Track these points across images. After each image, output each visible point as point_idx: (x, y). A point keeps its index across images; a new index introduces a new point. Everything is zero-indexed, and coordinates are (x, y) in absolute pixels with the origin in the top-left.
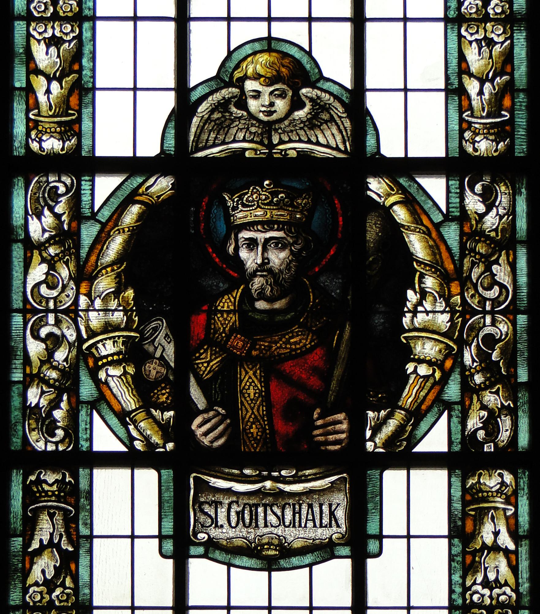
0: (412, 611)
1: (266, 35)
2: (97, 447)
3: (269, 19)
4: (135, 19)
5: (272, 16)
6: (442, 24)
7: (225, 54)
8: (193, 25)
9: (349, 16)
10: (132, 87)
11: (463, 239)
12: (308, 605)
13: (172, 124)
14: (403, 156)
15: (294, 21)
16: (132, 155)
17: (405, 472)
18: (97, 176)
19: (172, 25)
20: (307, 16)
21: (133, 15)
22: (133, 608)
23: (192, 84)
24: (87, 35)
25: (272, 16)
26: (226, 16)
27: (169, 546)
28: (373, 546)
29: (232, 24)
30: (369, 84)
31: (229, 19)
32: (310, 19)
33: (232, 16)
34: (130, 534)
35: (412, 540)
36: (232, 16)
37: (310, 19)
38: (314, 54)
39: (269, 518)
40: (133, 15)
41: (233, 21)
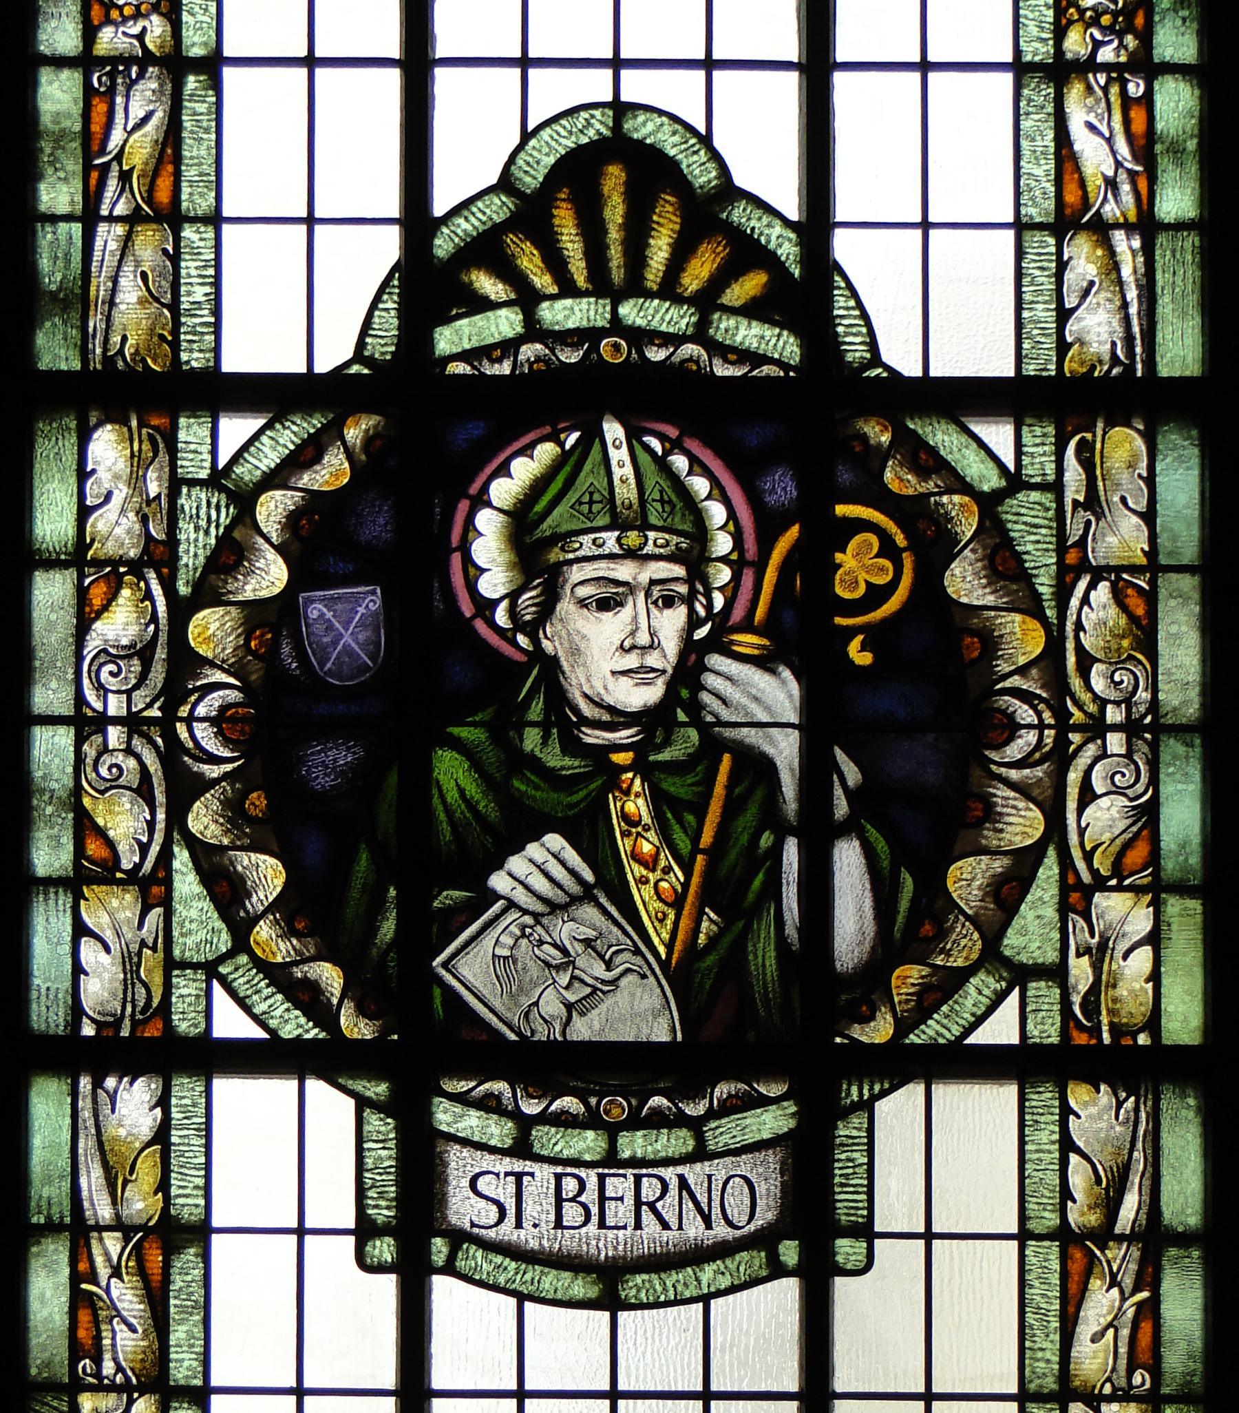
0: (622, 1403)
3: (617, 63)
4: (311, 62)
5: (715, 57)
6: (1008, 78)
7: (516, 140)
8: (441, 75)
10: (918, 219)
12: (607, 1388)
13: (390, 303)
14: (304, 370)
16: (304, 371)
19: (791, 81)
20: (702, 57)
21: (519, 55)
22: (928, 1397)
23: (439, 209)
26: (702, 57)
27: (384, 1249)
28: (847, 1250)
29: (320, 72)
32: (709, 64)
33: (624, 55)
35: (308, 1239)
36: (532, 54)
37: (709, 64)
38: (717, 143)
40: (519, 55)
41: (933, 70)
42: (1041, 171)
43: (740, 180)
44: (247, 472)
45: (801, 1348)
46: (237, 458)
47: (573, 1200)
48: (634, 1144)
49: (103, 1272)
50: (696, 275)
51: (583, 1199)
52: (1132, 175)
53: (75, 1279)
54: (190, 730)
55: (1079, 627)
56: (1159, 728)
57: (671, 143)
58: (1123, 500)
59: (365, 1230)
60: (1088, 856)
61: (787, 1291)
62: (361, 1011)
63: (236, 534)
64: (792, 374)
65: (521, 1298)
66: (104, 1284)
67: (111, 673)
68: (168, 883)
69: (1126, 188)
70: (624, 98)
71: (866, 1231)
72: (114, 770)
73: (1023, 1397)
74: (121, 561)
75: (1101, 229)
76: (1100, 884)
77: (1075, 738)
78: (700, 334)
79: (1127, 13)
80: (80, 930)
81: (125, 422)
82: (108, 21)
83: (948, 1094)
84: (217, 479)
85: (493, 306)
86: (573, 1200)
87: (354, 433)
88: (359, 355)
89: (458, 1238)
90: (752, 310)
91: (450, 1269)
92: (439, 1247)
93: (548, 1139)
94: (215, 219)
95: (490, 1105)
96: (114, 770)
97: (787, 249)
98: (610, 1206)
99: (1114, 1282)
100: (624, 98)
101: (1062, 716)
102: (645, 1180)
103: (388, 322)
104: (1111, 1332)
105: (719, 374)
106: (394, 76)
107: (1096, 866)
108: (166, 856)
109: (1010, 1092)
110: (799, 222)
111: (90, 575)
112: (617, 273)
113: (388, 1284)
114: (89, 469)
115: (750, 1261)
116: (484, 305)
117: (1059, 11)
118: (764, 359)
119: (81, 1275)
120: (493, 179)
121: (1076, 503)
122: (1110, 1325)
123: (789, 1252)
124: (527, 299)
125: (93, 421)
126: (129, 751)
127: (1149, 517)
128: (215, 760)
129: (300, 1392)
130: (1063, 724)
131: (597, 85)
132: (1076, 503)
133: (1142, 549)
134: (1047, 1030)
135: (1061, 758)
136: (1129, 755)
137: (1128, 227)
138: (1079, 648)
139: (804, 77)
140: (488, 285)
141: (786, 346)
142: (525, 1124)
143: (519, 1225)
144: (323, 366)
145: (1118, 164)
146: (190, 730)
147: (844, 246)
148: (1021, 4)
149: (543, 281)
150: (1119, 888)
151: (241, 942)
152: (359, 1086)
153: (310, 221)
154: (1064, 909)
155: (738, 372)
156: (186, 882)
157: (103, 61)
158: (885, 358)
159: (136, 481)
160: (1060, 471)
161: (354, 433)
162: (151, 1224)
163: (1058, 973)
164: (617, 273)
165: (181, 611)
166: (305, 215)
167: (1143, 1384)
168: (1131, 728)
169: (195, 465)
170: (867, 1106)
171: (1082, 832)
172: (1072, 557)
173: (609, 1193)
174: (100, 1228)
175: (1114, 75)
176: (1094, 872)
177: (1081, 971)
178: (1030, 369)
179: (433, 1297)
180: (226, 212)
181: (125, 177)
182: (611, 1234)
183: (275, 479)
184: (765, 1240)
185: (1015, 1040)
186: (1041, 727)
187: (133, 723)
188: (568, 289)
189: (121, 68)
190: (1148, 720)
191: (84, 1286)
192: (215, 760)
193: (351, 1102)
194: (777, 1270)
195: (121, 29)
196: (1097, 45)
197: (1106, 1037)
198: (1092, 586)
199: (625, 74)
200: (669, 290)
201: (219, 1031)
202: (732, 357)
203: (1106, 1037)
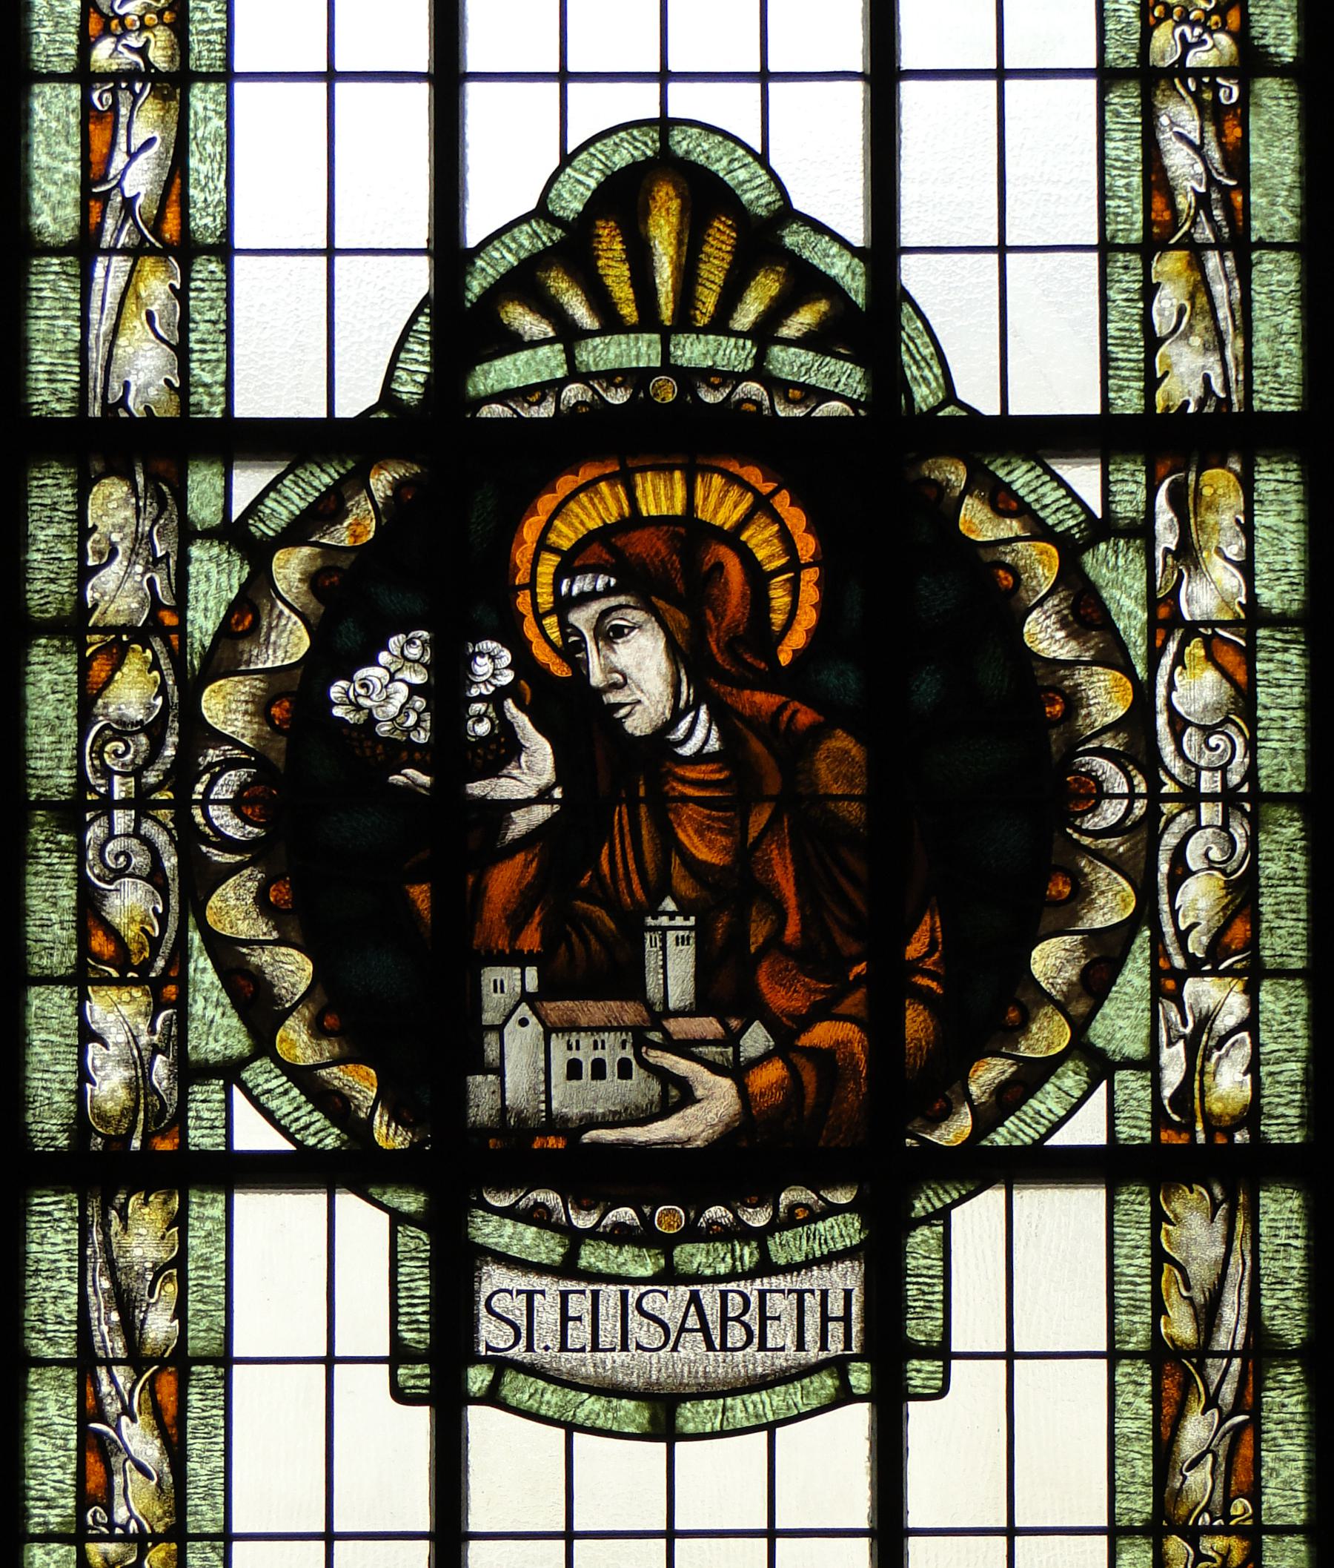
1: (656, 114)
3: (664, 76)
7: (555, 162)
9: (426, 70)
11: (1206, 629)
14: (323, 414)
17: (321, 1198)
21: (325, 69)
23: (472, 240)
24: (206, 125)
26: (757, 69)
28: (920, 1372)
30: (908, 236)
31: (564, 77)
33: (1008, 65)
34: (324, 1354)
38: (774, 162)
39: (632, 1325)
40: (325, 69)
42: (1129, 182)
43: (797, 205)
47: (737, 1319)
48: (694, 1256)
49: (113, 1408)
50: (748, 313)
51: (746, 1318)
53: (83, 1418)
54: (206, 814)
56: (1258, 797)
57: (719, 161)
59: (399, 1354)
60: (1182, 937)
61: (858, 1418)
62: (396, 1117)
64: (862, 412)
65: (571, 1428)
67: (115, 752)
68: (183, 982)
70: (662, 1446)
71: (942, 1352)
72: (122, 859)
76: (1194, 968)
77: (1167, 808)
78: (759, 372)
79: (1221, 10)
80: (87, 1035)
81: (128, 476)
82: (106, 31)
83: (1030, 1200)
85: (534, 344)
86: (737, 1319)
87: (381, 483)
89: (501, 1365)
90: (811, 341)
91: (493, 1397)
92: (478, 1378)
95: (537, 1217)
96: (122, 859)
98: (772, 1328)
99: (128, 204)
102: (730, 1295)
103: (420, 355)
104: (1210, 1457)
105: (782, 414)
107: (1191, 951)
108: (181, 953)
109: (1096, 1197)
111: (92, 644)
113: (421, 1416)
114: (90, 525)
115: (826, 1384)
117: (1144, 11)
119: (89, 1411)
120: (531, 204)
121: (1167, 551)
122: (1208, 1451)
123: (860, 1378)
124: (569, 334)
125: (97, 466)
126: (136, 834)
127: (1246, 568)
129: (771, 1534)
130: (1155, 797)
131: (643, 102)
132: (1167, 551)
133: (1240, 603)
134: (1136, 1130)
135: (1150, 827)
136: (1225, 827)
137: (1220, 246)
138: (1174, 716)
142: (575, 1238)
143: (530, 1348)
144: (348, 408)
145: (1211, 181)
146: (206, 814)
147: (913, 273)
148: (1107, 6)
150: (1215, 973)
151: (263, 1045)
152: (391, 1198)
153: (330, 252)
154: (1157, 993)
157: (105, 77)
158: (961, 395)
161: (381, 483)
162: (167, 1355)
163: (1150, 1065)
165: (191, 688)
166: (324, 246)
167: (100, 99)
168: (1228, 798)
170: (943, 1215)
171: (1174, 914)
172: (1163, 612)
173: (571, 1313)
174: (110, 1363)
175: (1206, 80)
176: (1189, 958)
179: (868, 1479)
182: (601, 1355)
183: (295, 533)
184: (838, 1366)
185: (1095, 409)
187: (141, 804)
188: (612, 323)
189: (124, 85)
190: (1245, 789)
191: (93, 1425)
193: (384, 1218)
194: (844, 1396)
196: (1187, 46)
197: (1201, 1138)
198: (1183, 644)
200: (720, 325)
201: (239, 1145)
203: (1201, 1138)
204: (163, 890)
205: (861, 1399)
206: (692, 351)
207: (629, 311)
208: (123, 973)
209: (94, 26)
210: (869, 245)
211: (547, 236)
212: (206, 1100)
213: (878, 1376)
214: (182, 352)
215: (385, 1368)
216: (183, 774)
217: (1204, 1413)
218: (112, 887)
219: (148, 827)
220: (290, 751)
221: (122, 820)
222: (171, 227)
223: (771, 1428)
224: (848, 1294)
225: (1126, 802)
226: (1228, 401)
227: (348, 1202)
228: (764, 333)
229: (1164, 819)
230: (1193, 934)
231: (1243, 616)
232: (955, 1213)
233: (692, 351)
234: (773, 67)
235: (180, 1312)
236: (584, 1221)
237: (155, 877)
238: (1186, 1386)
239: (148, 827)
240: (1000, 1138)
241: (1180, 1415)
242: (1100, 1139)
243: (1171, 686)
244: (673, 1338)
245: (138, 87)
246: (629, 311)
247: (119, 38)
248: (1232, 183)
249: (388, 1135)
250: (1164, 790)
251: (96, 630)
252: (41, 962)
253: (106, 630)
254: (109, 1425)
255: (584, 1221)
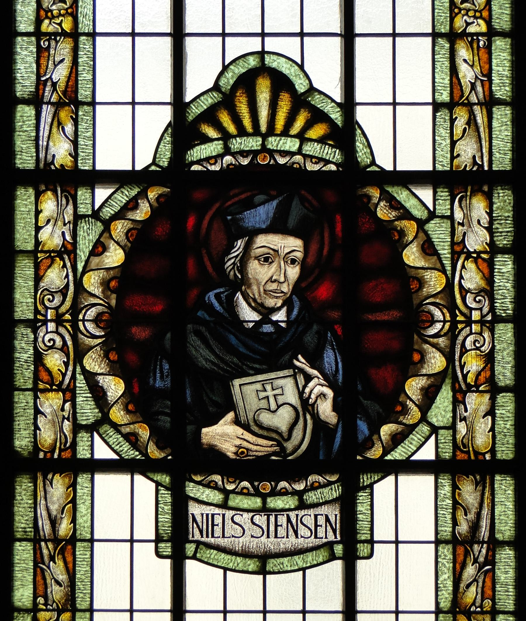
2: (97, 456)
3: (263, 35)
7: (220, 68)
12: (391, 32)
13: (168, 138)
15: (273, 36)
16: (131, 169)
18: (98, 188)
19: (168, 40)
23: (188, 99)
25: (266, 32)
27: (166, 548)
28: (363, 549)
29: (137, 39)
31: (224, 35)
35: (391, 101)
36: (226, 32)
38: (306, 68)
41: (99, 36)
44: (108, 212)
45: (343, 592)
46: (427, 439)
49: (46, 559)
52: (482, 81)
55: (461, 277)
57: (285, 68)
58: (479, 222)
59: (158, 540)
63: (102, 240)
64: (341, 169)
65: (225, 570)
66: (47, 563)
69: (479, 89)
70: (261, 577)
72: (52, 342)
73: (438, 611)
74: (53, 251)
75: (469, 105)
84: (96, 215)
85: (211, 140)
87: (152, 194)
88: (154, 163)
90: (322, 140)
92: (190, 548)
93: (235, 501)
94: (437, 106)
97: (336, 116)
99: (54, 85)
100: (261, 577)
101: (453, 316)
106: (338, 40)
108: (73, 377)
109: (431, 478)
110: (341, 103)
112: (263, 128)
115: (322, 555)
116: (207, 140)
118: (327, 162)
120: (211, 85)
123: (339, 549)
124: (226, 137)
126: (57, 332)
128: (94, 337)
130: (454, 323)
131: (255, 44)
135: (75, 309)
139: (343, 39)
140: (211, 133)
141: (336, 156)
144: (139, 167)
149: (232, 129)
150: (477, 391)
153: (394, 104)
155: (316, 168)
156: (445, 251)
158: (378, 162)
159: (471, 430)
160: (452, 209)
161: (152, 194)
164: (263, 128)
166: (131, 101)
168: (482, 322)
169: (84, 209)
170: (371, 486)
177: (462, 428)
178: (439, 168)
180: (98, 100)
181: (54, 85)
183: (119, 215)
184: (330, 545)
186: (84, 320)
187: (59, 320)
188: (242, 132)
189: (53, 37)
192: (94, 337)
193: (154, 485)
194: (333, 557)
195: (53, 21)
196: (468, 24)
197: (473, 457)
199: (266, 39)
200: (285, 133)
201: (97, 456)
202: (314, 160)
204: (68, 355)
205: (339, 558)
206: (273, 143)
207: (249, 128)
208: (51, 387)
209: (42, 13)
210: (343, 102)
211: (216, 97)
212: (83, 438)
213: (345, 550)
214: (75, 143)
215: (153, 544)
216: (75, 309)
217: (472, 565)
218: (45, 353)
219: (61, 330)
220: (412, 342)
221: (51, 326)
222: (460, 550)
223: (304, 570)
224: (336, 515)
225: (442, 324)
226: (482, 166)
227: (139, 478)
228: (301, 137)
229: (458, 330)
230: (469, 375)
231: (488, 250)
232: (375, 486)
233: (273, 143)
234: (266, 31)
235: (74, 521)
236: (230, 487)
237: (64, 349)
238: (467, 554)
239: (61, 330)
240: (389, 457)
241: (464, 566)
242: (432, 457)
243: (461, 277)
244: (299, 522)
245: (58, 38)
246: (249, 128)
247: (51, 19)
248: (486, 79)
249: (154, 452)
250: (458, 319)
251: (42, 251)
252: (19, 381)
253: (46, 252)
254: (46, 566)
255: (230, 487)
